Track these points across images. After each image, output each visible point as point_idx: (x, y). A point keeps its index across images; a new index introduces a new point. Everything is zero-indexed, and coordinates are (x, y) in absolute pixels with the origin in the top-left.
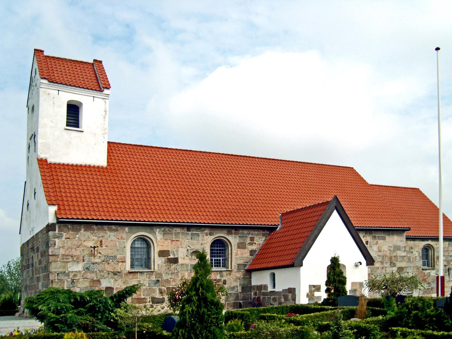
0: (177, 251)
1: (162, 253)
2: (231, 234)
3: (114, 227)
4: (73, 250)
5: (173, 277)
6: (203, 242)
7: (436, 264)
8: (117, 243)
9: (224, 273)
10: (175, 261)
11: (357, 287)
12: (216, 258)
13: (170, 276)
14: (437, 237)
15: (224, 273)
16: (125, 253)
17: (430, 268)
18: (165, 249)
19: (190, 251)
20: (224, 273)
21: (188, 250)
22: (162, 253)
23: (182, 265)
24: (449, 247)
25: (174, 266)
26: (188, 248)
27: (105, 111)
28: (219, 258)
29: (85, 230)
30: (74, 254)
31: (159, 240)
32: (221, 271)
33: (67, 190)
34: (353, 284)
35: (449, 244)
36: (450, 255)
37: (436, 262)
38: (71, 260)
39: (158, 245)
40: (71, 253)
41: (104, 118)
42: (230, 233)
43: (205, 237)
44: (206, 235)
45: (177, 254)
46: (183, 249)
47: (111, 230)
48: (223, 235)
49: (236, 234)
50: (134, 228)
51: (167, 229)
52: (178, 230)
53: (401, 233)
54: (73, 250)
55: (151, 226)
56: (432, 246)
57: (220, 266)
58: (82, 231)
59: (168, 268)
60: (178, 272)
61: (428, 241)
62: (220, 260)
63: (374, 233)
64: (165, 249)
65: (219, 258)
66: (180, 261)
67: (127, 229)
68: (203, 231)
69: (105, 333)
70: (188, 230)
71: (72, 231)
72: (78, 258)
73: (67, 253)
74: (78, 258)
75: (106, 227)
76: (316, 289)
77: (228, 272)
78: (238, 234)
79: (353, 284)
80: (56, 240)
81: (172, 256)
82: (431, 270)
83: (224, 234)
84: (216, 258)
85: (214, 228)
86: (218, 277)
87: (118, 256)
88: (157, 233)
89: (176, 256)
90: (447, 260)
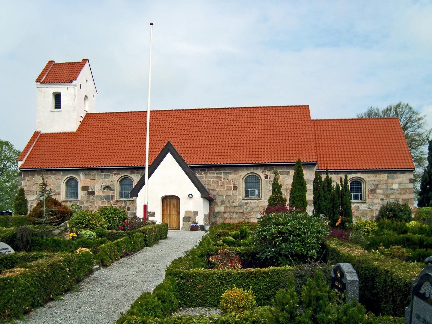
0: (94, 187)
1: (85, 188)
2: (134, 173)
3: (54, 172)
4: (31, 187)
5: (91, 204)
6: (112, 180)
7: (369, 198)
8: (56, 183)
9: (128, 203)
10: (92, 193)
11: (192, 215)
12: (355, 194)
13: (89, 204)
14: (144, 166)
15: (128, 203)
16: (60, 189)
17: (363, 201)
18: (86, 185)
19: (103, 187)
20: (128, 202)
21: (101, 186)
22: (85, 188)
23: (97, 196)
24: (388, 179)
25: (92, 197)
26: (102, 184)
27: (75, 95)
28: (357, 194)
29: (38, 175)
30: (32, 190)
31: (82, 180)
32: (126, 201)
33: (383, 153)
34: (186, 212)
35: (388, 177)
36: (389, 188)
37: (368, 196)
38: (30, 193)
39: (81, 183)
40: (30, 189)
41: (75, 100)
42: (132, 173)
43: (114, 176)
44: (115, 175)
45: (94, 189)
46: (98, 185)
47: (52, 174)
48: (127, 174)
49: (137, 173)
50: (66, 172)
51: (87, 172)
52: (95, 172)
53: (309, 167)
54: (31, 187)
55: (76, 170)
56: (363, 179)
57: (358, 199)
58: (36, 176)
59: (88, 199)
60: (94, 201)
61: (357, 174)
62: (358, 195)
63: (276, 168)
64: (86, 186)
65: (357, 194)
66: (96, 194)
67: (61, 173)
68: (112, 172)
69: (123, 238)
70: (102, 172)
71: (31, 176)
72: (33, 192)
73: (28, 190)
74: (33, 192)
75: (49, 172)
76: (150, 215)
77: (131, 202)
78: (140, 173)
79: (186, 212)
80: (22, 182)
81: (90, 190)
82: (360, 204)
83: (128, 173)
84: (355, 194)
85: (120, 169)
86: (123, 205)
87: (56, 191)
88: (81, 175)
89: (93, 191)
90: (385, 193)
